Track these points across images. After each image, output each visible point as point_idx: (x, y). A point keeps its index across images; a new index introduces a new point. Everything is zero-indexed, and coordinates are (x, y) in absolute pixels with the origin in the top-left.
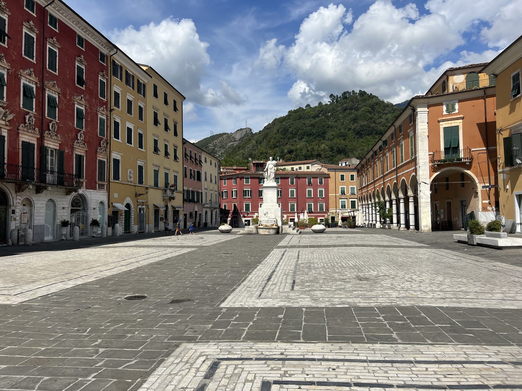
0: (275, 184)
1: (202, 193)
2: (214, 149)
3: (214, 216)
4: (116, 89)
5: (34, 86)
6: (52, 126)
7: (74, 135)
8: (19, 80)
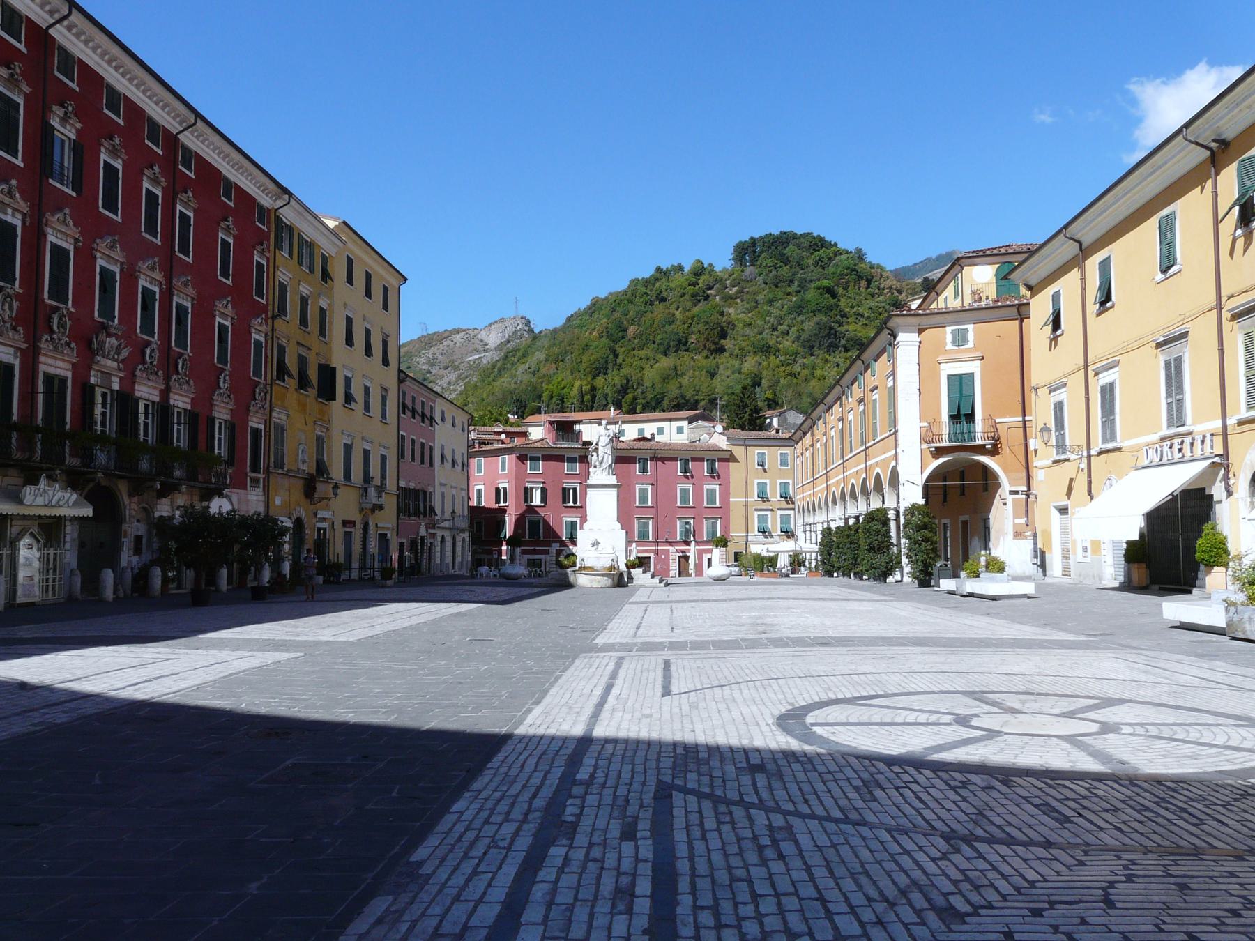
0: (613, 480)
3: (459, 549)
4: (283, 276)
5: (157, 290)
8: (136, 279)
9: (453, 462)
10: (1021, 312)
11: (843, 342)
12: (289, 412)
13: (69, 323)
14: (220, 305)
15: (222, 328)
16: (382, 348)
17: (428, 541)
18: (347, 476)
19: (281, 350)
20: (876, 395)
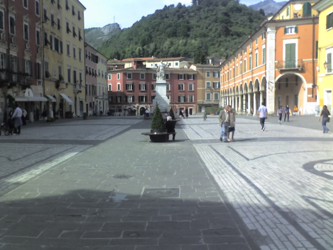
0: (165, 82)
6: (14, 40)
9: (103, 75)
10: (315, 20)
11: (231, 33)
12: (50, 55)
14: (24, 17)
15: (26, 26)
16: (78, 33)
17: (96, 103)
18: (69, 80)
19: (46, 34)
20: (257, 52)
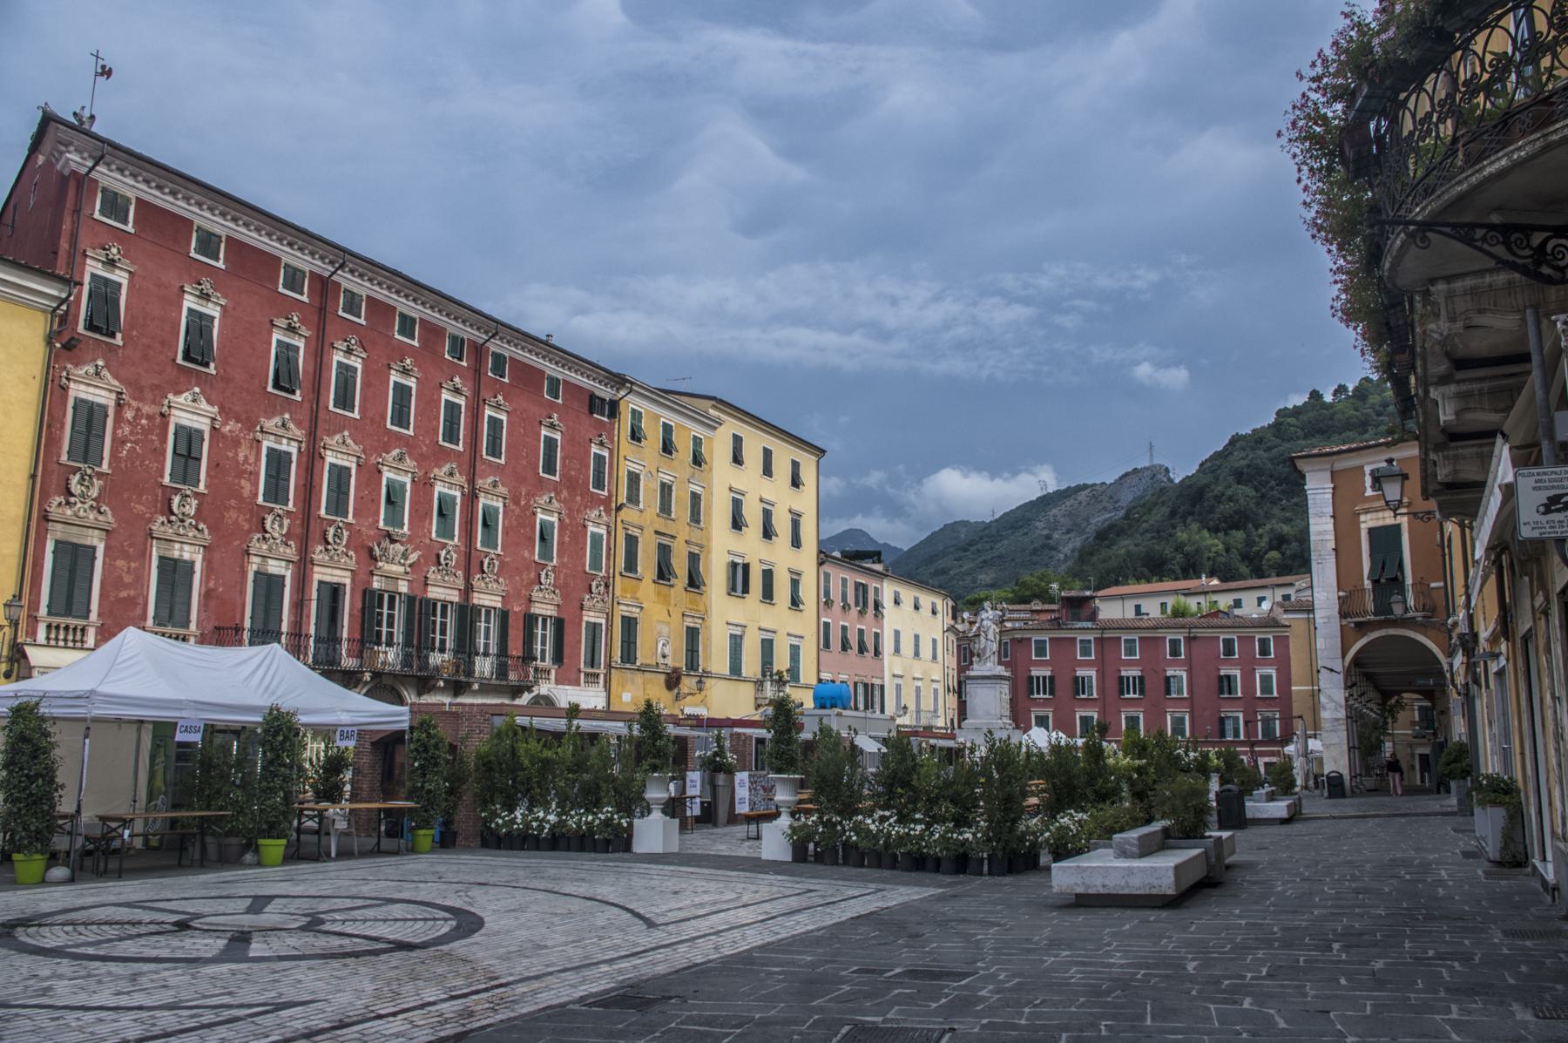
0: (1001, 670)
1: (882, 687)
2: (1049, 537)
7: (532, 575)
13: (346, 533)
